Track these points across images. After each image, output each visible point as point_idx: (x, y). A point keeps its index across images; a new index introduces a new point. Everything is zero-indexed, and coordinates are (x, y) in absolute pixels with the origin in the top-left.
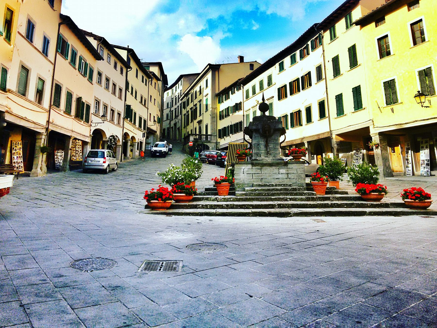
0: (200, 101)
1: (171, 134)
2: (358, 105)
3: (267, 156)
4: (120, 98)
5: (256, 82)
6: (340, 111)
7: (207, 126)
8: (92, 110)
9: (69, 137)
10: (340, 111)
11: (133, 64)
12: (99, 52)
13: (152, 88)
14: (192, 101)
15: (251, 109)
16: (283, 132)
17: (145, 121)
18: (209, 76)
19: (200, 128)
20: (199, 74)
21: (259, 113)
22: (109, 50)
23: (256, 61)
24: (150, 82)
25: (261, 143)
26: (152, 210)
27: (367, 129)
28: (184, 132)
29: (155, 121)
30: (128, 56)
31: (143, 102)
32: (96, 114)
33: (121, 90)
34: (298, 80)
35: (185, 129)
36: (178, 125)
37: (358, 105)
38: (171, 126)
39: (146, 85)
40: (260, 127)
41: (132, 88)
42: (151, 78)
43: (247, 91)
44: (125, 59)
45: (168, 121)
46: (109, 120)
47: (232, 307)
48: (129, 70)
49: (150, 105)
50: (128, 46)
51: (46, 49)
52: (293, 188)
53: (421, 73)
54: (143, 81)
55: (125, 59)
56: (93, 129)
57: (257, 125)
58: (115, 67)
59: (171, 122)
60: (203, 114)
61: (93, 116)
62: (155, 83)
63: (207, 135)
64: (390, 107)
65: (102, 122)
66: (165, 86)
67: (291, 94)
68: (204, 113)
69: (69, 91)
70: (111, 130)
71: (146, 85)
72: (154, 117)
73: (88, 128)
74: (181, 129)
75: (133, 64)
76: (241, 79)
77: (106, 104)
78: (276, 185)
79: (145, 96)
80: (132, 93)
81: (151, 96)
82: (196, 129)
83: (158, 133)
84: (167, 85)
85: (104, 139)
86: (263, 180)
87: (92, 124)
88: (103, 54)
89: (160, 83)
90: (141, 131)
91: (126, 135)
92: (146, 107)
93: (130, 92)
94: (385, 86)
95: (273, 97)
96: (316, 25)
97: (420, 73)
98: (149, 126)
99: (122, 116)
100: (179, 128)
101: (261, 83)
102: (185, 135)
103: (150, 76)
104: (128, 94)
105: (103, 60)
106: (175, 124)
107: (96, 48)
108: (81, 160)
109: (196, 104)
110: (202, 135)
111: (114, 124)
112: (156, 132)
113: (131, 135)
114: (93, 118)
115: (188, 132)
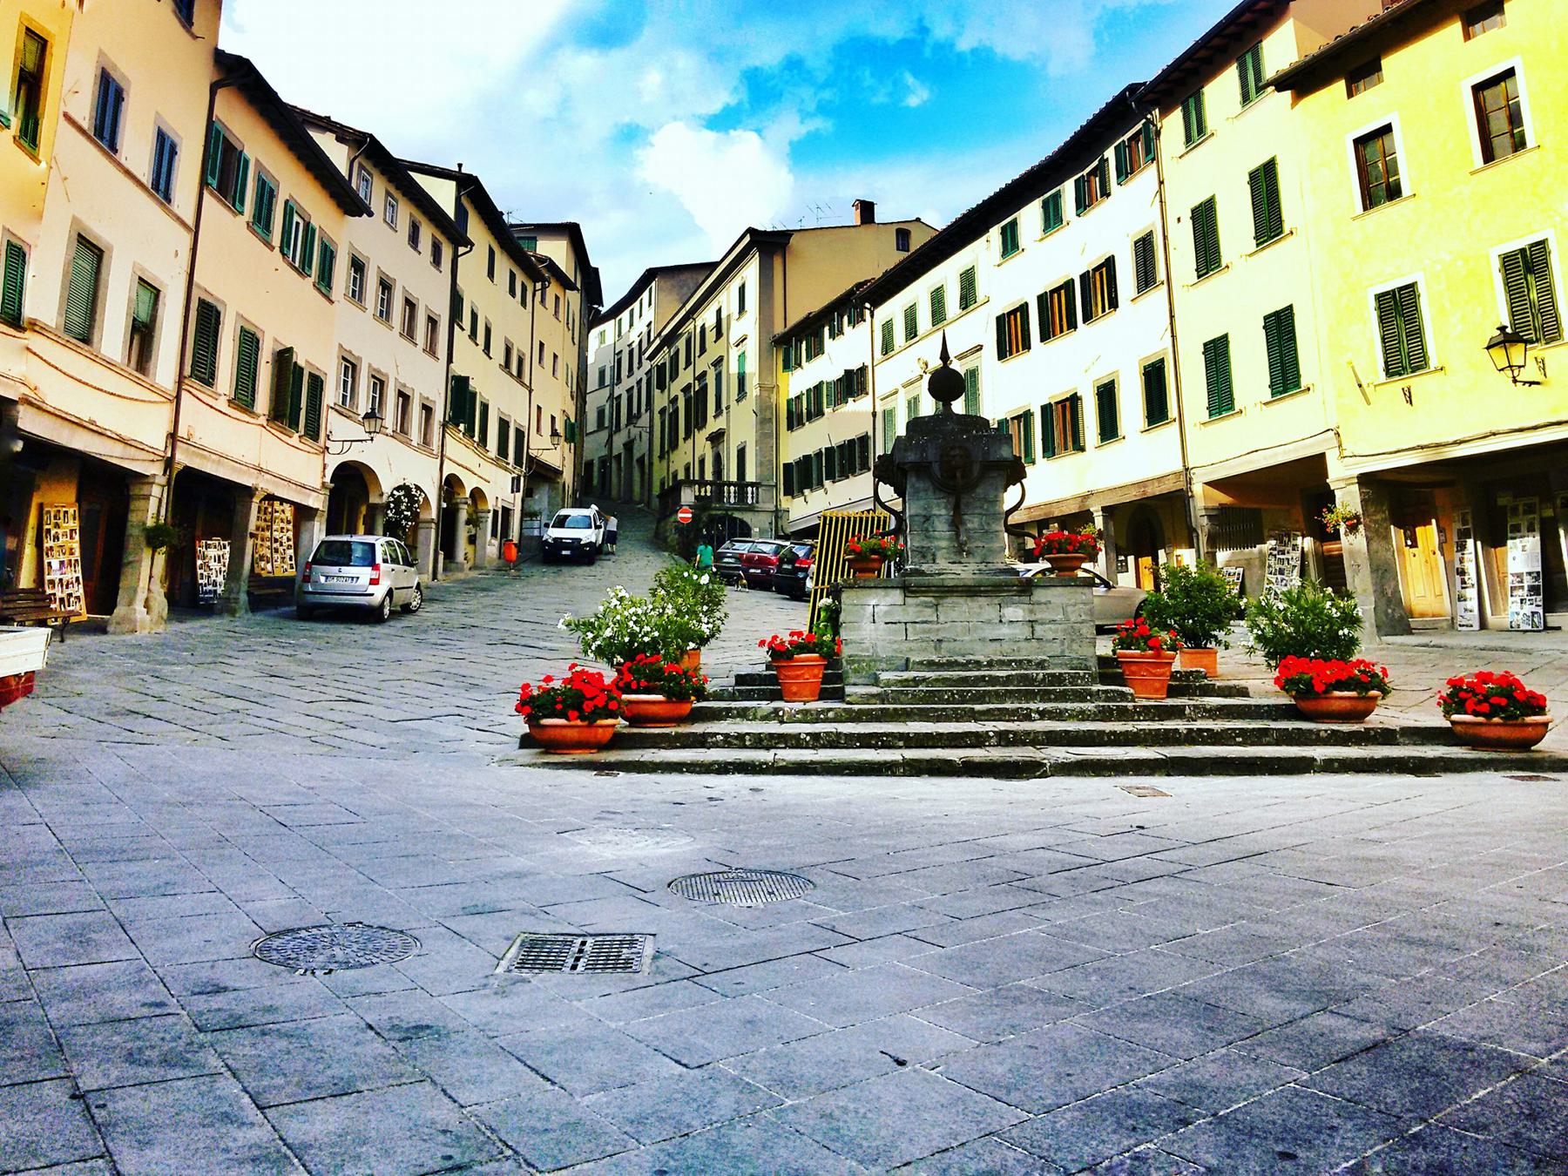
0: (718, 362)
1: (614, 479)
2: (1285, 375)
3: (957, 559)
4: (431, 350)
5: (918, 293)
6: (1221, 399)
7: (741, 453)
8: (331, 395)
9: (249, 492)
10: (1221, 399)
11: (476, 229)
12: (354, 185)
13: (544, 315)
14: (688, 363)
15: (902, 391)
16: (1015, 472)
17: (520, 434)
18: (750, 272)
19: (718, 459)
20: (714, 265)
21: (928, 406)
22: (390, 181)
23: (918, 220)
24: (539, 294)
25: (935, 512)
26: (546, 753)
27: (1318, 461)
28: (659, 472)
29: (554, 433)
30: (458, 199)
31: (515, 367)
32: (345, 408)
33: (433, 322)
34: (1068, 286)
35: (665, 462)
36: (640, 449)
37: (1285, 375)
38: (615, 453)
39: (524, 303)
40: (931, 454)
41: (474, 316)
42: (543, 280)
43: (888, 328)
44: (450, 211)
45: (604, 435)
46: (389, 431)
47: (831, 1102)
48: (462, 250)
49: (540, 375)
50: (460, 166)
51: (163, 176)
52: (1053, 675)
53: (1510, 263)
54: (512, 292)
55: (450, 211)
56: (333, 462)
57: (923, 449)
58: (414, 240)
59: (615, 438)
60: (728, 408)
61: (332, 414)
62: (557, 298)
63: (741, 484)
64: (1398, 384)
65: (367, 436)
66: (590, 309)
67: (1045, 337)
68: (733, 404)
69: (248, 327)
70: (399, 466)
71: (524, 303)
72: (553, 418)
73: (317, 461)
74: (651, 464)
75: (476, 229)
76: (866, 282)
77: (379, 372)
78: (990, 664)
79: (522, 345)
80: (473, 335)
81: (542, 345)
82: (702, 462)
83: (568, 477)
84: (601, 303)
85: (374, 499)
86: (944, 645)
87: (329, 444)
88: (369, 195)
89: (574, 298)
90: (506, 469)
91: (451, 485)
92: (523, 384)
93: (468, 331)
94: (1380, 308)
95: (980, 348)
96: (1133, 88)
97: (1508, 261)
98: (533, 453)
99: (438, 416)
100: (641, 461)
101: (937, 298)
102: (662, 484)
103: (539, 271)
104: (461, 337)
105: (370, 214)
106: (629, 446)
107: (344, 171)
108: (291, 572)
109: (704, 374)
110: (725, 484)
111: (408, 444)
112: (559, 473)
113: (470, 483)
114: (333, 422)
115: (675, 475)
